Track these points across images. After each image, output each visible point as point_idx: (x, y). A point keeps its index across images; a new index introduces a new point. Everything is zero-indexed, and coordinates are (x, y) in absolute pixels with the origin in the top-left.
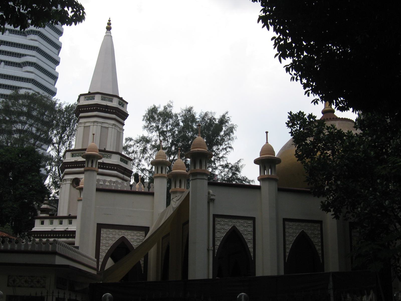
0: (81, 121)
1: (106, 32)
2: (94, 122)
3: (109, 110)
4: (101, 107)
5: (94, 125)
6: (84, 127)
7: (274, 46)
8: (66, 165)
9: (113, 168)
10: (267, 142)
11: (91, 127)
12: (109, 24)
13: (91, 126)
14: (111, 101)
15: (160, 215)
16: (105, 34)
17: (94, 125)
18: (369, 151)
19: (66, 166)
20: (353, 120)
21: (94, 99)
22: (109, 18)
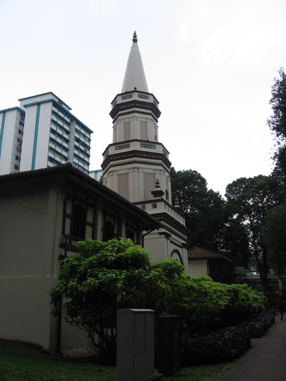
0: (120, 118)
7: (54, 304)
8: (111, 157)
9: (158, 157)
12: (135, 36)
16: (132, 46)
18: (261, 192)
20: (218, 194)
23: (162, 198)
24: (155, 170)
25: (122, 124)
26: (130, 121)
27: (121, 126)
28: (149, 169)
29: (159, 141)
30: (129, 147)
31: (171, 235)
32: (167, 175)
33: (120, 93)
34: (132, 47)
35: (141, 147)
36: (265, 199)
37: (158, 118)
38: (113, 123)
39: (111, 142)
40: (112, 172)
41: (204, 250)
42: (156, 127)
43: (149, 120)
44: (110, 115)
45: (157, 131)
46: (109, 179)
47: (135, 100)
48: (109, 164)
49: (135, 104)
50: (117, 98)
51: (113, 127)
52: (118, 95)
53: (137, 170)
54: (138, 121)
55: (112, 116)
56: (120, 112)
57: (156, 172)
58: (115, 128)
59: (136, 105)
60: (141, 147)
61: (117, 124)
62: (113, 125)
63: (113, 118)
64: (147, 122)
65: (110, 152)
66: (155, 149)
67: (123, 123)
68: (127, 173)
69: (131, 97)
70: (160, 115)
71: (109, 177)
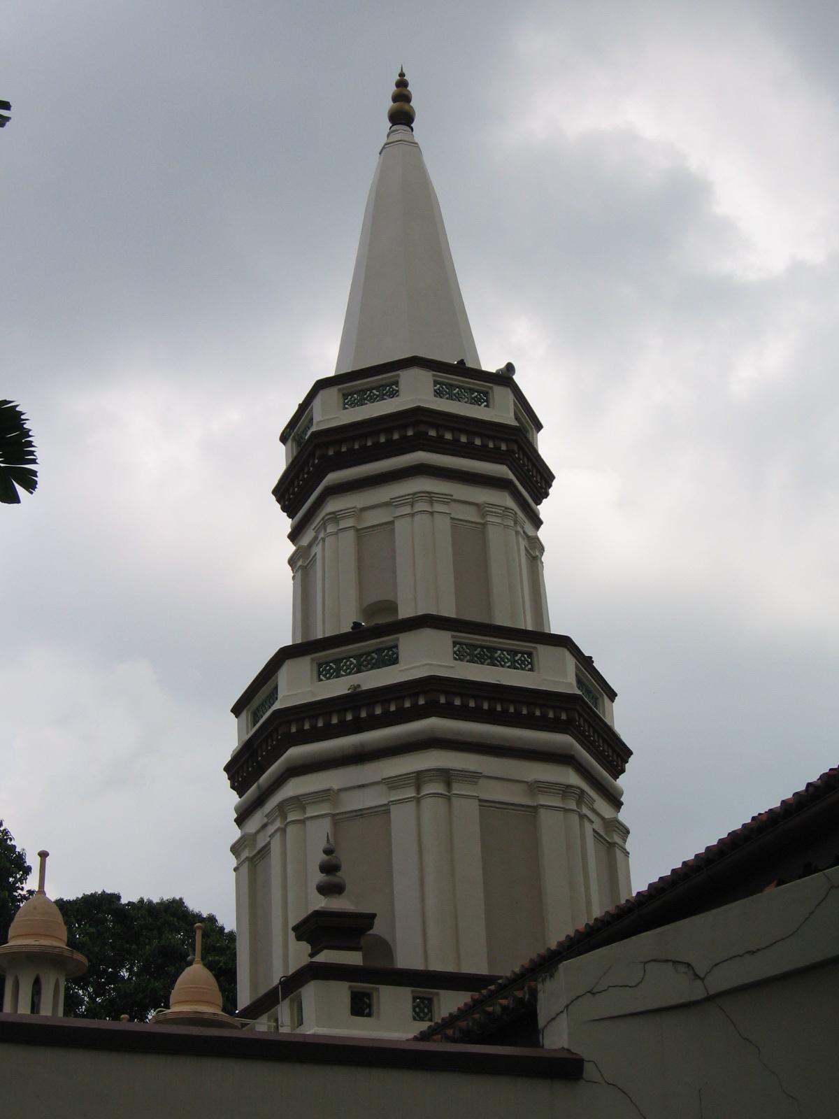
2: (414, 498)
4: (447, 428)
5: (412, 515)
11: (402, 818)
12: (402, 94)
13: (393, 809)
15: (435, 373)
17: (412, 515)
19: (293, 730)
24: (536, 787)
25: (349, 539)
26: (392, 522)
27: (336, 549)
28: (506, 780)
29: (556, 628)
30: (394, 661)
32: (607, 817)
33: (331, 372)
34: (383, 148)
35: (459, 656)
37: (538, 502)
38: (294, 536)
39: (286, 638)
40: (298, 802)
42: (535, 549)
43: (496, 514)
44: (279, 501)
45: (540, 571)
46: (323, 550)
47: (418, 411)
48: (282, 759)
49: (415, 428)
50: (317, 403)
51: (292, 562)
52: (321, 385)
53: (438, 788)
54: (437, 516)
55: (289, 500)
56: (333, 477)
57: (490, 519)
58: (301, 563)
59: (438, 702)
60: (455, 659)
61: (315, 538)
62: (235, 833)
63: (291, 515)
64: (535, 809)
65: (282, 692)
66: (531, 670)
67: (351, 533)
68: (384, 811)
69: (394, 394)
70: (550, 486)
71: (283, 830)
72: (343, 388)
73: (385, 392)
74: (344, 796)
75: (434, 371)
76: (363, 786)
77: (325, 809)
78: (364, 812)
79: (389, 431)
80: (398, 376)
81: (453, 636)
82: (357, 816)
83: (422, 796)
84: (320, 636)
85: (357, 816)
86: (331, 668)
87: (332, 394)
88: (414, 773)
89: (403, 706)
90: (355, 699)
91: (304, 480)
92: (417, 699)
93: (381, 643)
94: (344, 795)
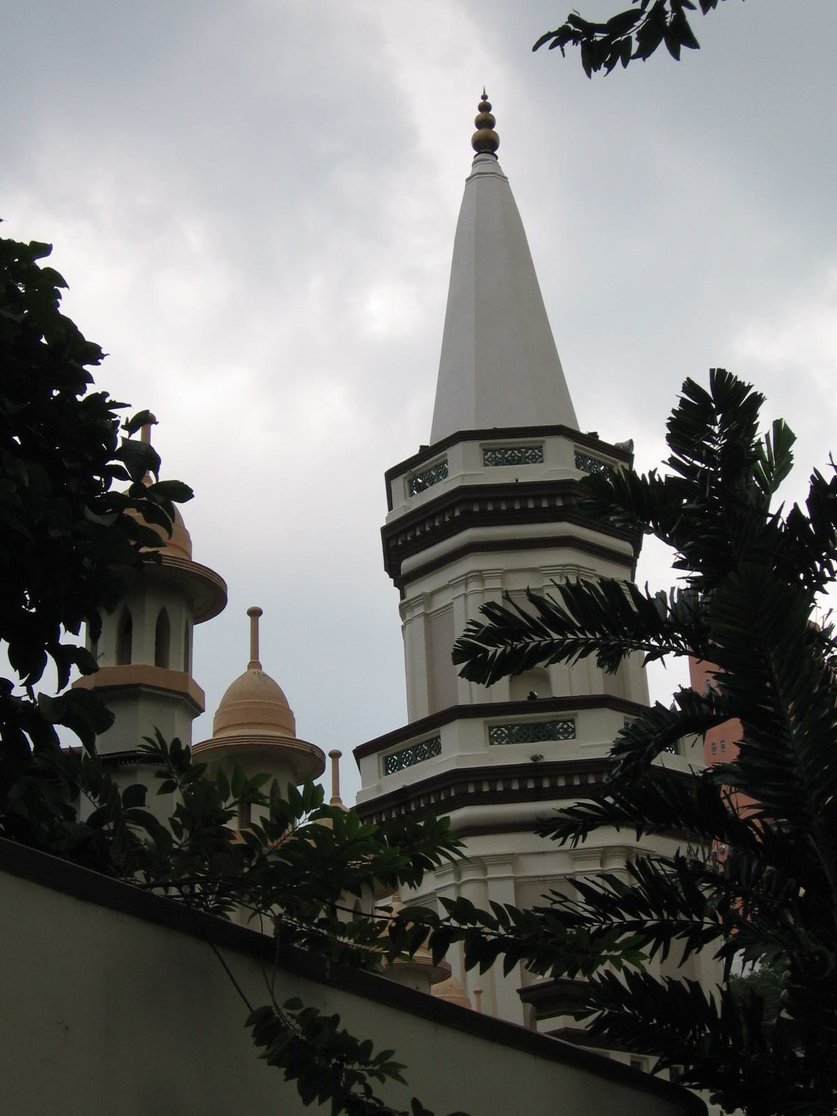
1: (473, 160)
2: (466, 579)
3: (504, 507)
5: (466, 595)
6: (426, 615)
10: (255, 664)
12: (485, 121)
14: (537, 458)
15: (577, 444)
21: (445, 473)
22: (482, 94)
23: (635, 57)
31: (448, 818)
35: (493, 740)
36: (327, 974)
41: (163, 561)
72: (485, 444)
73: (527, 455)
74: (525, 861)
75: (575, 441)
76: (543, 853)
77: (506, 872)
78: (546, 879)
79: (523, 499)
80: (543, 442)
81: (625, 718)
82: (539, 881)
83: (464, 883)
84: (467, 702)
85: (539, 881)
86: (503, 732)
87: (474, 447)
88: (602, 847)
89: (511, 787)
90: (537, 769)
91: (414, 537)
92: (573, 780)
93: (557, 716)
94: (523, 860)
